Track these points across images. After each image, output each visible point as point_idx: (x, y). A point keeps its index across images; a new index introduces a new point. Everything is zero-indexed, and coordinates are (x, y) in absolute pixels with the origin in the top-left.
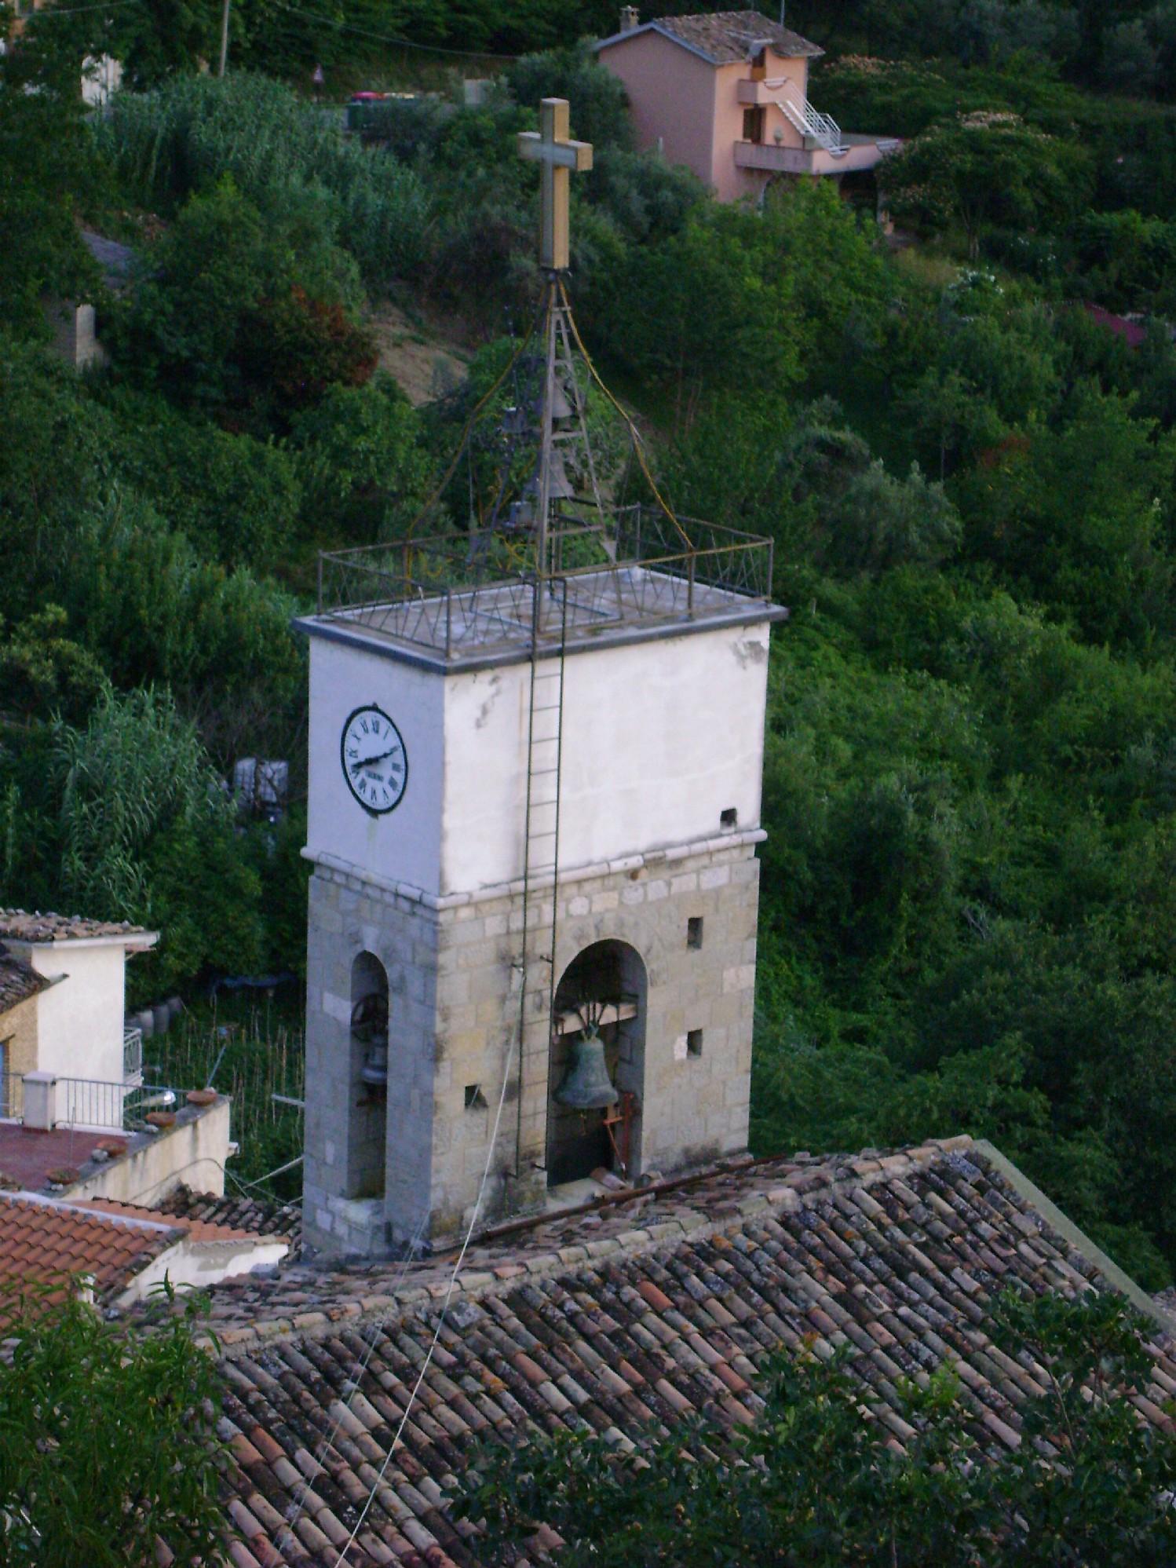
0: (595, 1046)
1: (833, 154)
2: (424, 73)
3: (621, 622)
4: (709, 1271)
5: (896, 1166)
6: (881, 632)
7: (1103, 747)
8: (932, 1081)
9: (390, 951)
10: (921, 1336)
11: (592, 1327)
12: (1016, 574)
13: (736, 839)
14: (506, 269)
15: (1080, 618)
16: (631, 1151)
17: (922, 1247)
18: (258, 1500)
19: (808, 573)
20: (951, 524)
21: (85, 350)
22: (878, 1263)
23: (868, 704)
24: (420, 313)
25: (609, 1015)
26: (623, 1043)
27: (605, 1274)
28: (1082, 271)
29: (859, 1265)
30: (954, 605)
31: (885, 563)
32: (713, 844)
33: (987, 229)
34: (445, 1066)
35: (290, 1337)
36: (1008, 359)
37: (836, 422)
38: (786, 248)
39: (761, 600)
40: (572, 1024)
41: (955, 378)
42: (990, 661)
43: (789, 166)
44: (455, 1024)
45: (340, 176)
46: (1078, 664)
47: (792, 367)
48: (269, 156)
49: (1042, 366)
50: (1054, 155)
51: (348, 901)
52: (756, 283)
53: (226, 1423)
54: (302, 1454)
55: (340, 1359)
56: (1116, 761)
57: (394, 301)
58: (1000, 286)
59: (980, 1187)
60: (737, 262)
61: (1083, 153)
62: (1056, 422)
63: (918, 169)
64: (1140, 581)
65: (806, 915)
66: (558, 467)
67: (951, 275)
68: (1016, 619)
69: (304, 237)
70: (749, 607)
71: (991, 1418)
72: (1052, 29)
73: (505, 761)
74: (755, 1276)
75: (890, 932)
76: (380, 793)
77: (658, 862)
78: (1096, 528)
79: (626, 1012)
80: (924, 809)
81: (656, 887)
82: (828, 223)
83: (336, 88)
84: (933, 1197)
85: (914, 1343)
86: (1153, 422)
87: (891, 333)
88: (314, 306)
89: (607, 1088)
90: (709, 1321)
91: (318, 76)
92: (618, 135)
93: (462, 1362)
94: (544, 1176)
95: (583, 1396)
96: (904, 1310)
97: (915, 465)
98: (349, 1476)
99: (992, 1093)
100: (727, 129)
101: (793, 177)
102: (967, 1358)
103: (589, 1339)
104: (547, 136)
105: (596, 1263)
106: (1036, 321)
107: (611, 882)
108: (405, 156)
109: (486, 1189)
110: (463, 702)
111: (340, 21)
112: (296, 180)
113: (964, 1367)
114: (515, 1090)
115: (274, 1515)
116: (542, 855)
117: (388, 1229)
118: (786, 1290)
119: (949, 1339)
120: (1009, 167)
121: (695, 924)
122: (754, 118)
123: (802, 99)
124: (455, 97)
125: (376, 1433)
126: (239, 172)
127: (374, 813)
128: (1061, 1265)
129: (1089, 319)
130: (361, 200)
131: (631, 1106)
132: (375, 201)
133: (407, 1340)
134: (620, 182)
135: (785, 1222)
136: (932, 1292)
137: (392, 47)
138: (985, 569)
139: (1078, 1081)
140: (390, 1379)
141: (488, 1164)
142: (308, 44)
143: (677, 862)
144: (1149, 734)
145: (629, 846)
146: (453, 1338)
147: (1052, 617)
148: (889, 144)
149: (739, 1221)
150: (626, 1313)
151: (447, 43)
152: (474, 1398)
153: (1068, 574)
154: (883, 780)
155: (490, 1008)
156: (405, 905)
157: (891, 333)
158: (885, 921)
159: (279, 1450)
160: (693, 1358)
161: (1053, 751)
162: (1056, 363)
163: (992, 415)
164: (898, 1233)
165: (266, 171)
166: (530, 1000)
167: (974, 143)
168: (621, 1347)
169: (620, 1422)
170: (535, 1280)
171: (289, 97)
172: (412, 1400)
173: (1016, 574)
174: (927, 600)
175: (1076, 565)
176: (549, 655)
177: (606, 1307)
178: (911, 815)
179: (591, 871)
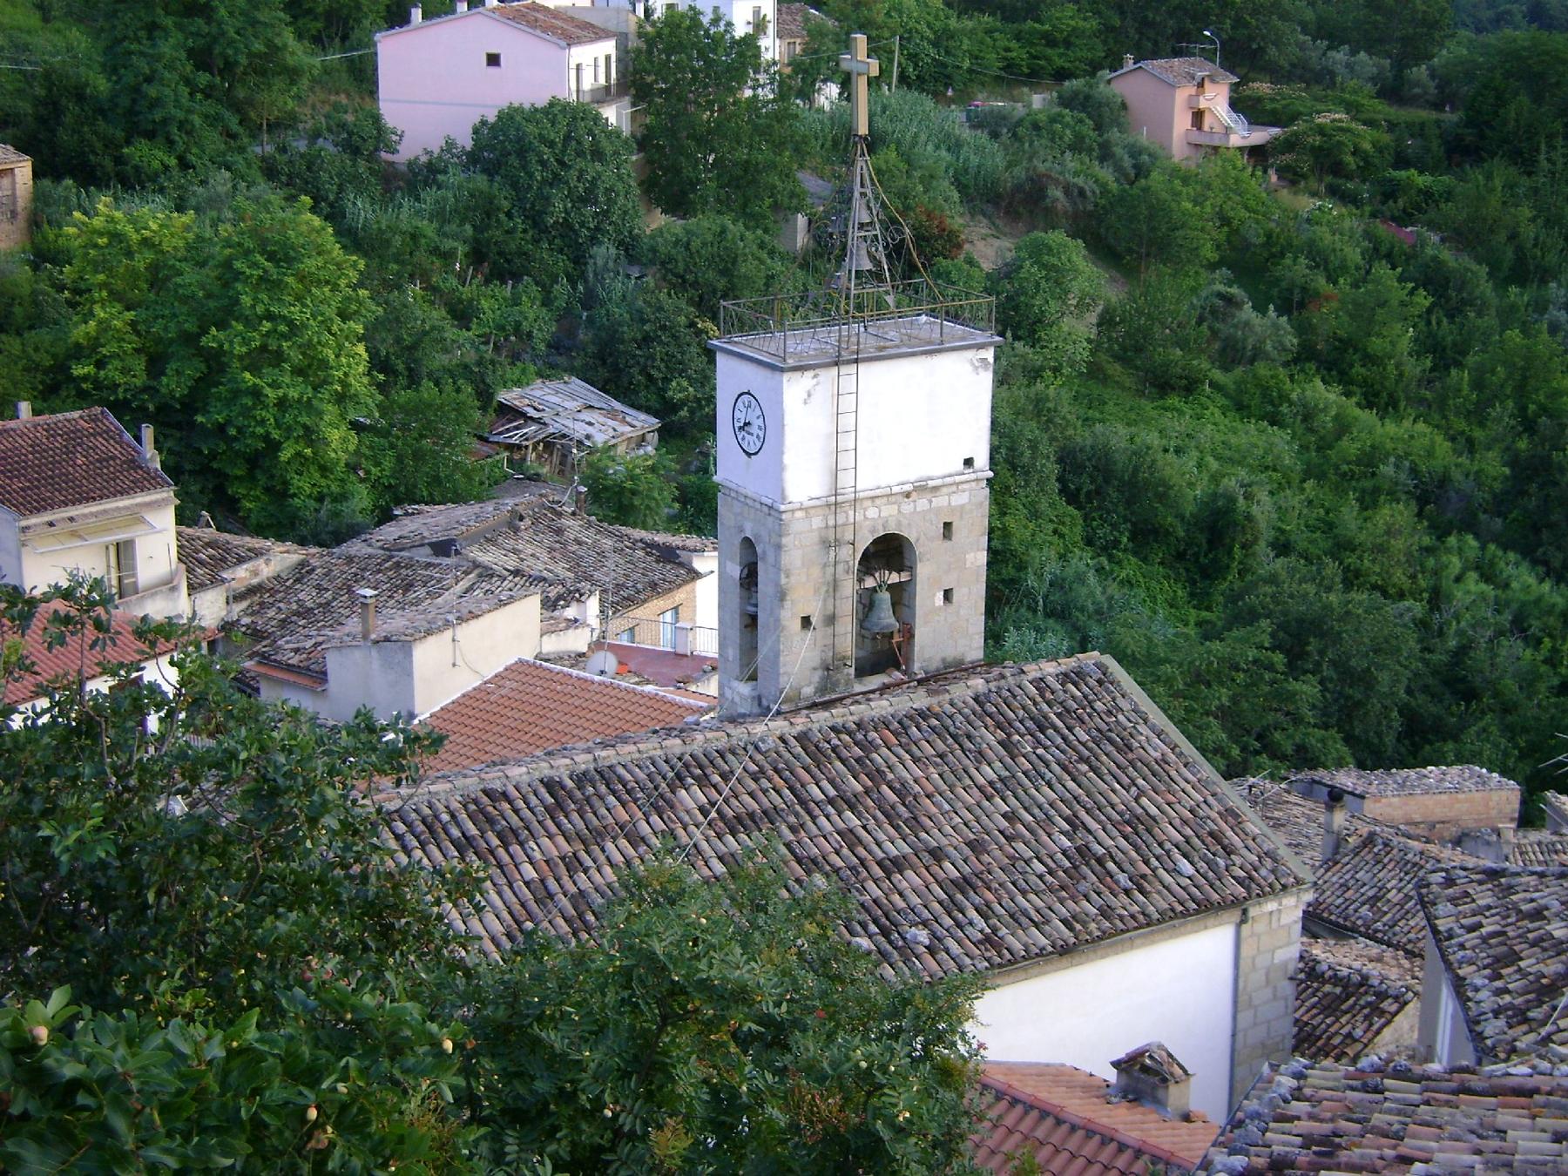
0: (885, 596)
1: (1243, 135)
2: (1015, 92)
3: (902, 344)
4: (924, 725)
5: (1050, 668)
6: (1245, 399)
7: (1367, 466)
8: (1216, 646)
9: (757, 536)
10: (1048, 766)
11: (845, 753)
12: (1329, 370)
13: (973, 476)
14: (1045, 197)
15: (1365, 395)
16: (909, 660)
17: (1058, 715)
18: (623, 842)
19: (1205, 365)
20: (1291, 341)
21: (801, 239)
22: (1029, 724)
23: (1233, 440)
24: (997, 222)
25: (894, 578)
26: (901, 596)
27: (859, 725)
28: (1383, 203)
29: (1018, 724)
30: (1288, 385)
31: (1252, 361)
32: (958, 479)
33: (1329, 179)
34: (788, 604)
35: (659, 752)
36: (1334, 250)
37: (1230, 284)
38: (1208, 186)
39: (988, 334)
40: (870, 583)
41: (1303, 260)
42: (1307, 417)
43: (1216, 143)
44: (793, 579)
45: (955, 146)
46: (1356, 419)
47: (1208, 252)
48: (916, 135)
49: (1354, 255)
50: (1367, 139)
51: (737, 507)
52: (1189, 205)
53: (611, 799)
54: (655, 818)
55: (686, 766)
56: (1373, 474)
57: (984, 215)
58: (1333, 209)
59: (1100, 682)
60: (1179, 194)
61: (1386, 138)
62: (1355, 285)
63: (1289, 145)
64: (1401, 375)
65: (1180, 556)
66: (864, 252)
67: (1307, 204)
68: (1323, 394)
69: (929, 180)
70: (981, 337)
71: (1082, 814)
72: (1375, 70)
73: (825, 426)
74: (952, 729)
75: (1228, 567)
76: (752, 444)
77: (922, 488)
78: (1376, 344)
79: (905, 577)
80: (1248, 497)
81: (922, 503)
82: (1233, 173)
83: (963, 98)
84: (1071, 687)
85: (1044, 770)
86: (1410, 285)
87: (1269, 235)
88: (929, 215)
89: (892, 620)
90: (918, 753)
91: (950, 93)
92: (1119, 125)
93: (762, 771)
94: (852, 671)
95: (832, 792)
96: (1040, 751)
97: (1271, 307)
98: (680, 832)
99: (1252, 654)
100: (1182, 123)
101: (1216, 149)
102: (1074, 780)
103: (843, 761)
104: (854, 57)
105: (855, 718)
106: (1351, 228)
107: (893, 499)
108: (995, 135)
109: (816, 677)
110: (795, 388)
111: (966, 64)
112: (930, 148)
113: (1071, 784)
114: (831, 620)
115: (631, 851)
116: (846, 480)
117: (759, 698)
118: (969, 737)
119: (1065, 768)
120: (1340, 143)
121: (947, 525)
122: (1198, 116)
123: (1226, 106)
124: (1029, 105)
125: (702, 809)
126: (899, 143)
127: (749, 455)
128: (1142, 728)
129: (1382, 229)
130: (967, 160)
131: (909, 633)
132: (975, 160)
133: (730, 757)
134: (1118, 151)
135: (976, 699)
136: (1059, 740)
137: (998, 79)
138: (1311, 367)
139: (1309, 648)
140: (716, 778)
141: (816, 662)
142: (948, 77)
143: (936, 488)
144: (1392, 459)
145: (904, 479)
146: (759, 757)
147: (1348, 394)
148: (1275, 131)
149: (947, 697)
150: (868, 747)
151: (1029, 76)
152: (765, 791)
153: (1358, 370)
154: (1226, 480)
155: (816, 572)
156: (765, 509)
157: (1269, 235)
158: (1225, 560)
159: (640, 815)
160: (905, 774)
161: (1337, 468)
162: (1362, 254)
163: (1322, 281)
164: (1045, 707)
165: (914, 144)
166: (840, 568)
167: (1321, 130)
168: (860, 766)
169: (852, 808)
170: (815, 727)
171: (929, 103)
172: (726, 791)
173: (1329, 370)
174: (1272, 382)
175: (1363, 366)
176: (849, 362)
177: (856, 744)
178: (1241, 500)
179: (878, 492)
